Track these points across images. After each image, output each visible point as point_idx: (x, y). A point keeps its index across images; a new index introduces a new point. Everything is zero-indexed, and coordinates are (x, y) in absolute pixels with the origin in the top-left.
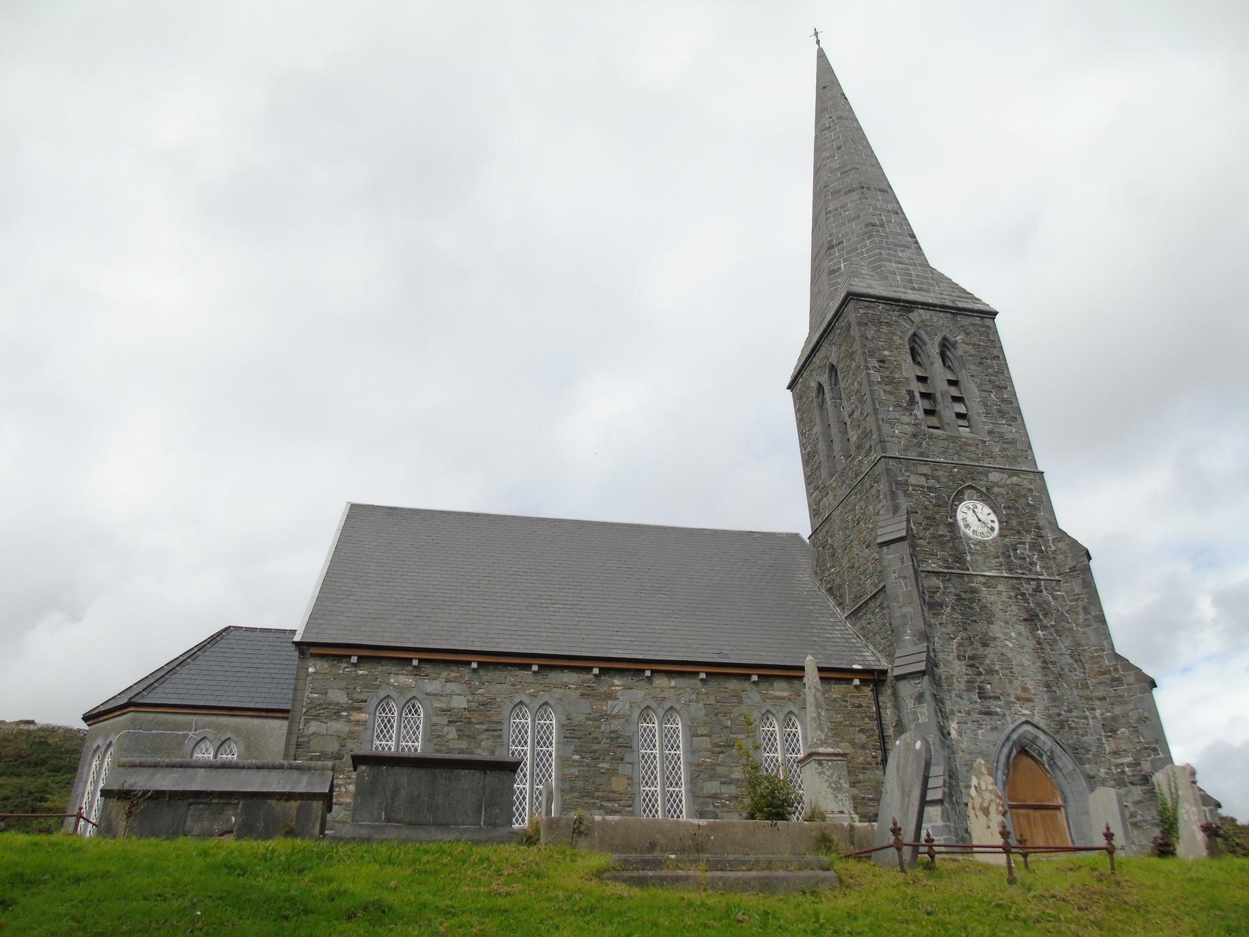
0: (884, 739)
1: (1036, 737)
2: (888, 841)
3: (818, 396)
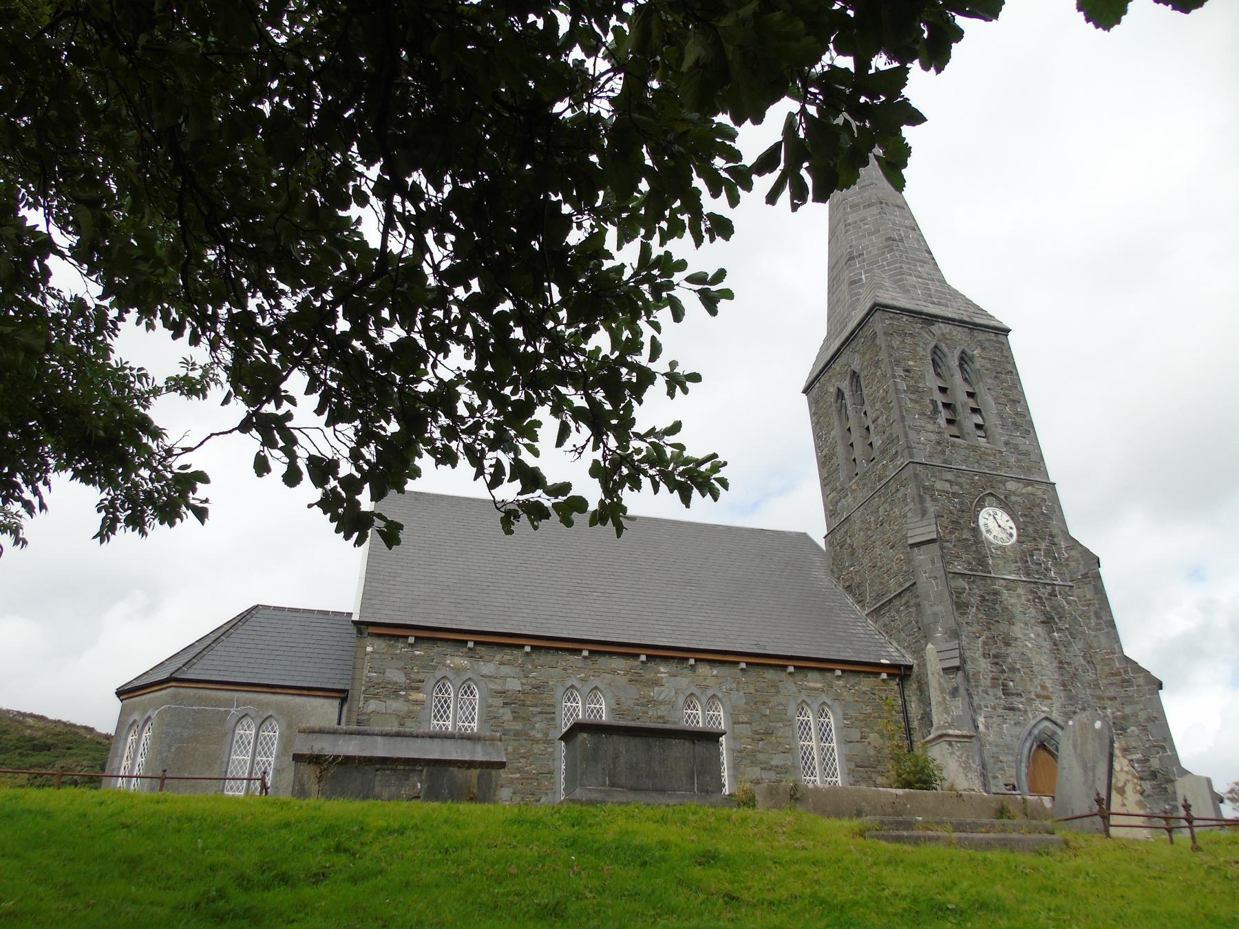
0: (910, 732)
1: (1055, 733)
2: (1073, 813)
3: (837, 401)
